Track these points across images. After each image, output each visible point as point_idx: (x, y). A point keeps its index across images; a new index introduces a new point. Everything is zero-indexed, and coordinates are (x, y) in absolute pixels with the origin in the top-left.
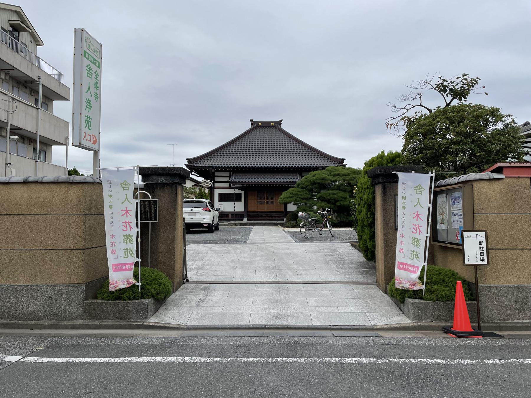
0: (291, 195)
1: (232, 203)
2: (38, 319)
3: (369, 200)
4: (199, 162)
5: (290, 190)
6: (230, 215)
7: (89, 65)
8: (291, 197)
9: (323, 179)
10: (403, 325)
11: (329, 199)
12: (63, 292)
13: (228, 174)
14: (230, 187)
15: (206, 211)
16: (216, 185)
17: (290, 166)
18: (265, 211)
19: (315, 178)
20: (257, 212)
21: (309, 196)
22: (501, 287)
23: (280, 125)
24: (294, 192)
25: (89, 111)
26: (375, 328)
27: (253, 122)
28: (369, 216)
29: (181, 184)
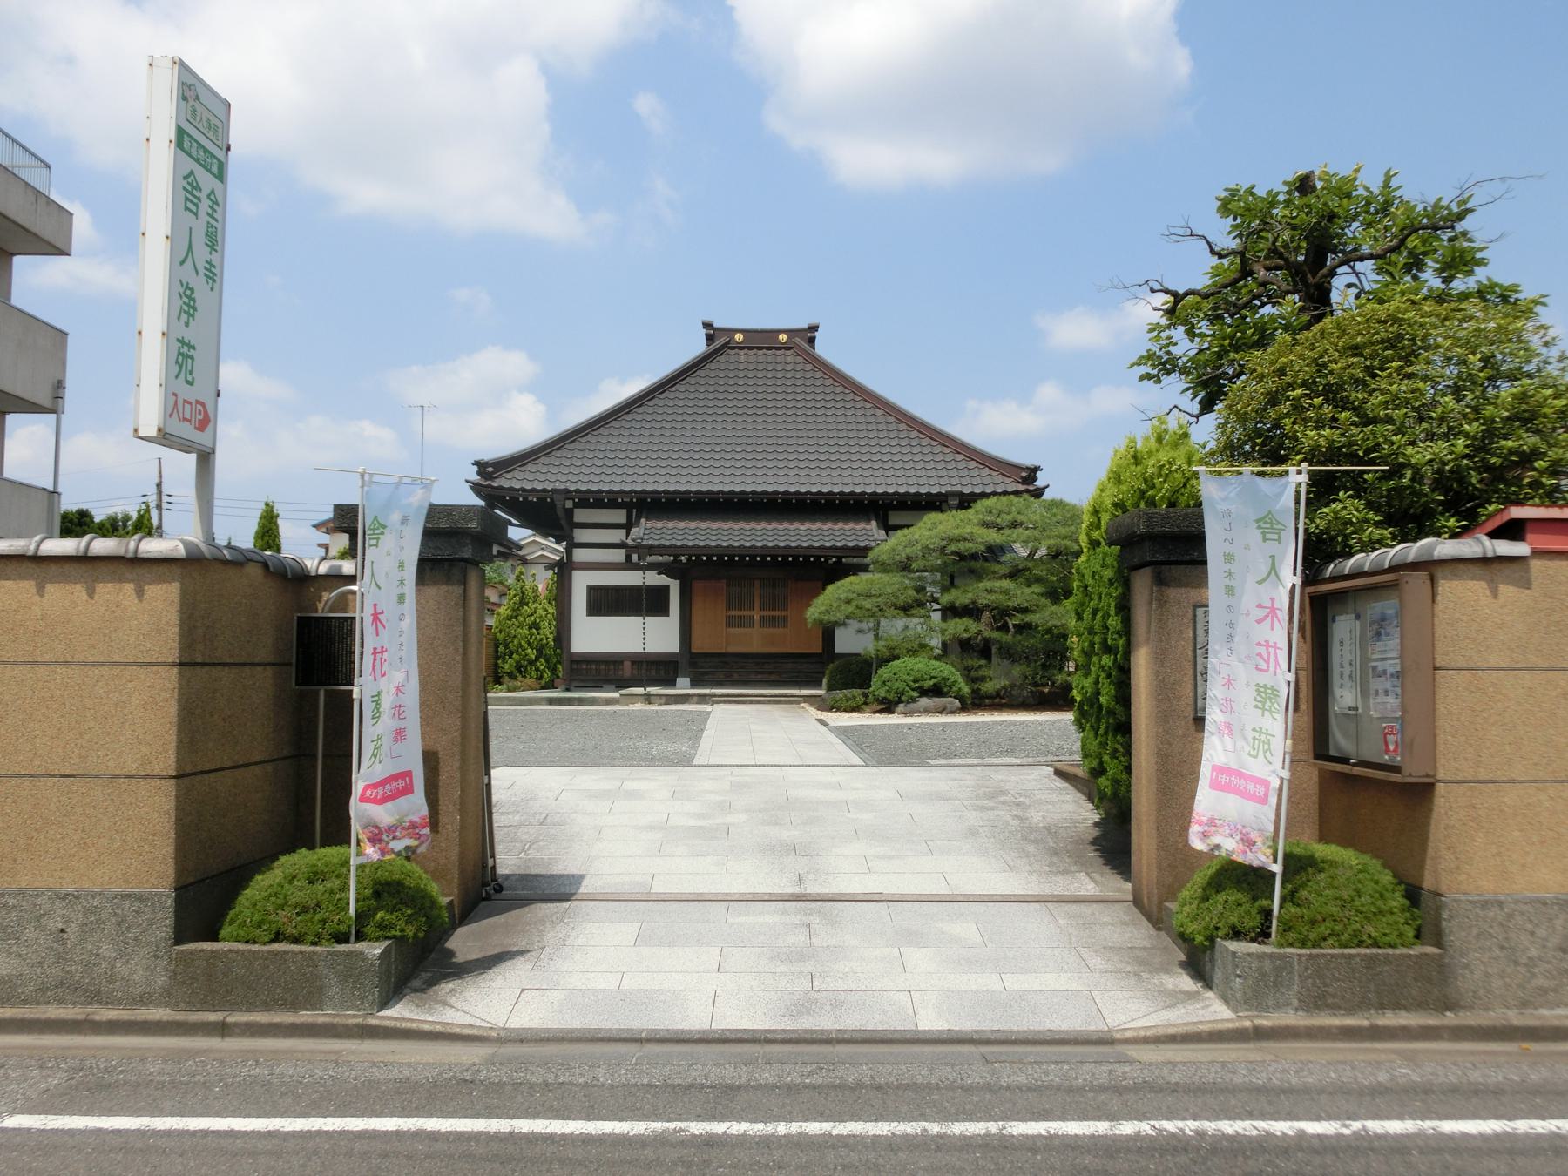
1: (635, 621)
2: (25, 1002)
6: (627, 664)
7: (192, 173)
10: (1206, 1027)
12: (104, 915)
13: (620, 516)
14: (628, 565)
16: (580, 555)
22: (1517, 902)
23: (812, 341)
25: (187, 325)
26: (1118, 1036)
29: (476, 564)
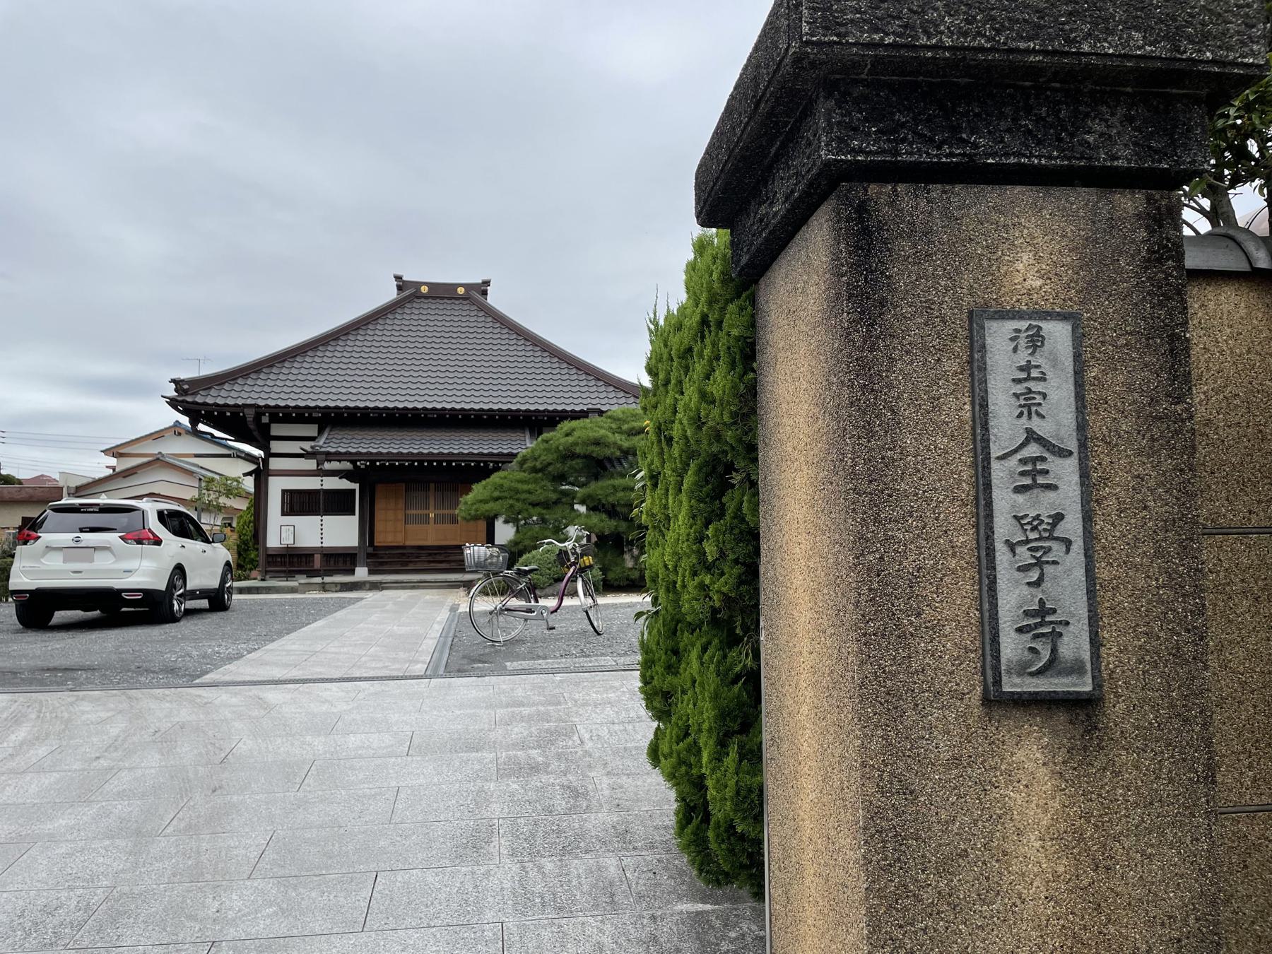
0: (496, 494)
3: (714, 416)
4: (213, 392)
5: (496, 478)
6: (317, 557)
8: (497, 499)
9: (597, 443)
11: (613, 506)
13: (311, 430)
14: (320, 473)
15: (139, 542)
16: (275, 464)
17: (505, 407)
18: (430, 542)
19: (570, 439)
20: (404, 547)
21: (554, 496)
23: (485, 293)
24: (506, 484)
27: (402, 285)
28: (710, 549)
